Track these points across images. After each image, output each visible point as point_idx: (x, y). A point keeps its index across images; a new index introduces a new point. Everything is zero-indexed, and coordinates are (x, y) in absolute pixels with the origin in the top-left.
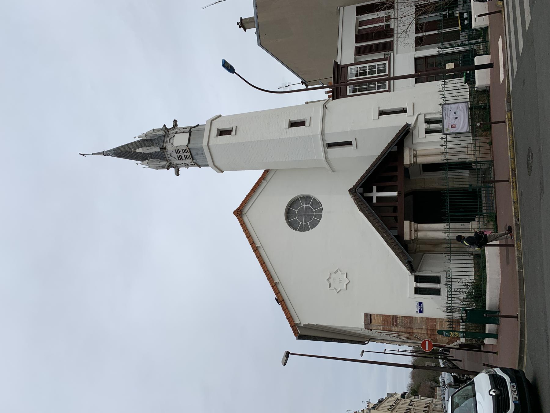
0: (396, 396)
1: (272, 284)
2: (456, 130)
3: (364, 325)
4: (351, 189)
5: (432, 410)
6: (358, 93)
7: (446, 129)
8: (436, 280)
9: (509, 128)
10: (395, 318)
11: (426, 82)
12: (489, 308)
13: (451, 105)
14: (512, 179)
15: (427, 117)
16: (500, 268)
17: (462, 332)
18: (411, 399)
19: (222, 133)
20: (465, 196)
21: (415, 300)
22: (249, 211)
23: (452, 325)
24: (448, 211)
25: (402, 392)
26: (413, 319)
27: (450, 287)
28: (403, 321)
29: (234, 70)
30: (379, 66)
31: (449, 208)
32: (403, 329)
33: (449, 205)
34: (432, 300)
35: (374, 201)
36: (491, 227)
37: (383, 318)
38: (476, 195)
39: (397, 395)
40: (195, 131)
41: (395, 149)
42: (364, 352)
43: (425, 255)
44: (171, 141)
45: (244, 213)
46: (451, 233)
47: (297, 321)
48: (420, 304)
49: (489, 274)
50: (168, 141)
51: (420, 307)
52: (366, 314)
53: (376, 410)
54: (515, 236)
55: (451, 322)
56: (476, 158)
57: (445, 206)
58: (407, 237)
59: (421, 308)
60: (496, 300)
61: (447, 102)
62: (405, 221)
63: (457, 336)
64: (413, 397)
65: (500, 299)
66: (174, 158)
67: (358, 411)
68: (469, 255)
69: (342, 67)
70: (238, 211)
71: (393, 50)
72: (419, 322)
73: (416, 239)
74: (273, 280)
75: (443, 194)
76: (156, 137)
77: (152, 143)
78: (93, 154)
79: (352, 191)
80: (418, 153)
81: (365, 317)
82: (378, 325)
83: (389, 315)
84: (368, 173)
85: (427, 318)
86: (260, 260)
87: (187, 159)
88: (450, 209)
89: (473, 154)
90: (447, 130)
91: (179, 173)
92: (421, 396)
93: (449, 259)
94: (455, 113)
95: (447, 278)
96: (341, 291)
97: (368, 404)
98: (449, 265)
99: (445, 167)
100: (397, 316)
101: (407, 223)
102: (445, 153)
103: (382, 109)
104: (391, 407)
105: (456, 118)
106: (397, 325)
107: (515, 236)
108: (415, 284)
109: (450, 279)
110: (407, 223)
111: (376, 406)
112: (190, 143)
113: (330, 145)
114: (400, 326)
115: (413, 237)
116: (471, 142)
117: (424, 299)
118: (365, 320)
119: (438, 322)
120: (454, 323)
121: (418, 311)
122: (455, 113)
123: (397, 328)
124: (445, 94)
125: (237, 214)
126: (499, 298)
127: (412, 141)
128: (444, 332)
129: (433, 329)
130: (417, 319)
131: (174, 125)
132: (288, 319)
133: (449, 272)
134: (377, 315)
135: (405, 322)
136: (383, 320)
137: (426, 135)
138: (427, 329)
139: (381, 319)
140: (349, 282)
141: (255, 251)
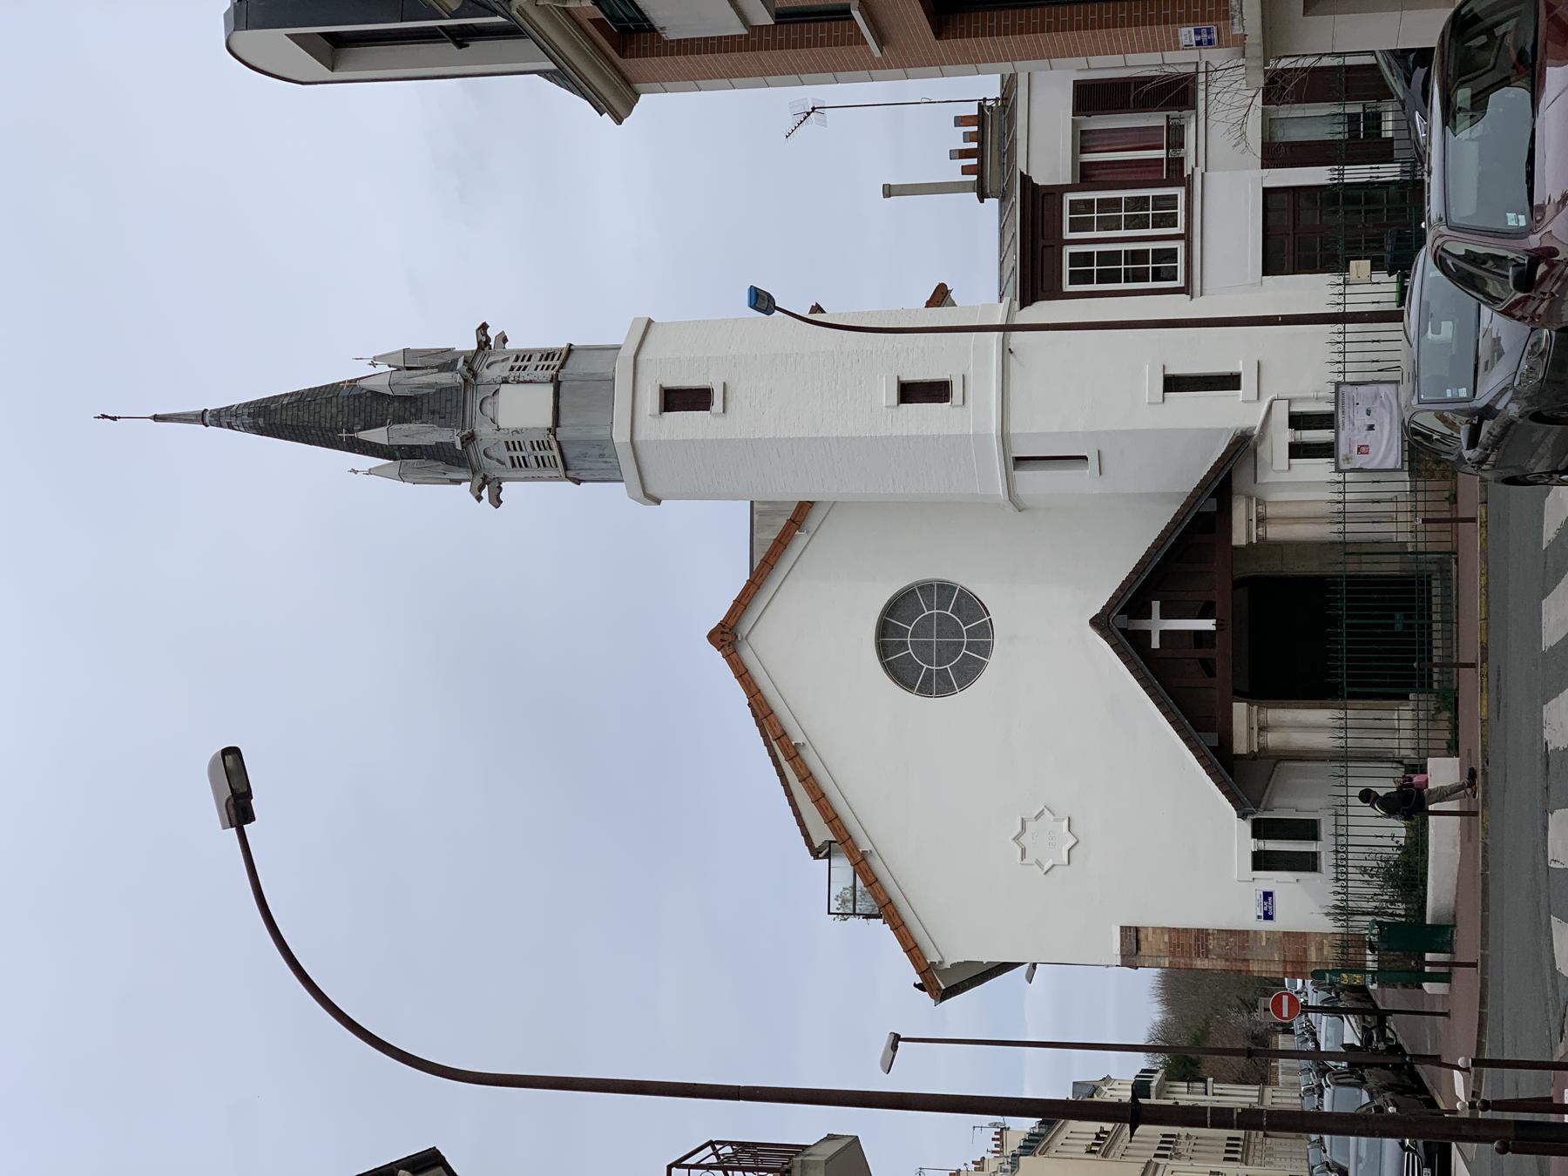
0: (1112, 1092)
1: (852, 857)
2: (1368, 463)
7: (1344, 455)
8: (1309, 830)
10: (1202, 935)
12: (1434, 916)
13: (1360, 388)
14: (1481, 667)
15: (1298, 408)
18: (1177, 1096)
19: (677, 399)
22: (756, 629)
24: (1342, 683)
25: (1138, 1073)
26: (1248, 935)
28: (1224, 943)
29: (770, 298)
32: (1223, 963)
33: (1347, 658)
34: (1297, 885)
35: (1155, 643)
36: (1445, 725)
37: (1170, 937)
39: (1115, 1086)
40: (575, 383)
41: (1212, 506)
43: (1281, 764)
44: (487, 407)
45: (742, 638)
47: (933, 957)
48: (1267, 895)
50: (484, 457)
51: (1266, 903)
52: (1124, 929)
53: (1039, 1158)
54: (1479, 795)
55: (1344, 947)
57: (1336, 669)
58: (1240, 747)
59: (1270, 907)
61: (1349, 378)
63: (1358, 981)
64: (1182, 1086)
65: (1457, 896)
66: (498, 461)
67: (964, 1168)
70: (722, 633)
71: (1194, 107)
72: (1264, 944)
73: (1263, 749)
74: (856, 847)
75: (1333, 636)
76: (426, 391)
77: (413, 410)
78: (156, 418)
80: (1271, 511)
81: (1121, 935)
82: (1157, 956)
84: (1142, 573)
85: (1284, 933)
90: (1347, 459)
93: (1340, 372)
94: (1368, 413)
97: (996, 1133)
100: (1207, 930)
101: (1240, 709)
103: (1175, 370)
104: (1098, 1138)
105: (1371, 428)
106: (1206, 955)
107: (1479, 795)
108: (1252, 845)
110: (1240, 709)
111: (1037, 1141)
113: (1020, 461)
114: (1215, 957)
115: (1256, 746)
116: (1406, 486)
118: (1122, 945)
119: (1313, 943)
120: (1351, 950)
121: (1262, 914)
123: (1206, 960)
125: (722, 640)
128: (1327, 975)
129: (1299, 960)
130: (1259, 936)
131: (479, 343)
133: (1343, 838)
135: (1227, 945)
136: (1170, 942)
138: (1285, 961)
139: (1166, 939)
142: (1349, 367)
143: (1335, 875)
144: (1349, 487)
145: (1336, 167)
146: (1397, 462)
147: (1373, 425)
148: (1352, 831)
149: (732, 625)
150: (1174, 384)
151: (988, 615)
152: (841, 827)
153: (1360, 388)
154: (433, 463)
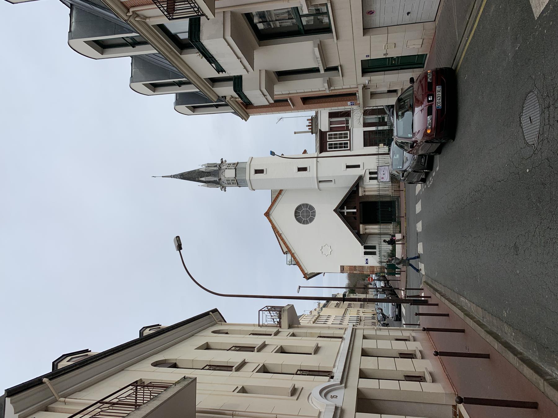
6: (333, 150)
8: (374, 247)
10: (355, 267)
15: (371, 171)
19: (257, 172)
21: (365, 258)
29: (274, 153)
30: (345, 134)
35: (345, 214)
38: (392, 204)
39: (340, 295)
41: (355, 189)
47: (306, 272)
48: (367, 259)
54: (405, 241)
58: (361, 233)
62: (360, 225)
71: (351, 116)
78: (163, 177)
80: (366, 190)
88: (381, 219)
91: (226, 190)
94: (383, 171)
95: (379, 251)
101: (361, 226)
102: (379, 190)
104: (337, 304)
105: (384, 174)
107: (405, 241)
108: (364, 250)
110: (361, 226)
113: (320, 181)
122: (383, 171)
131: (221, 162)
134: (346, 266)
142: (380, 187)
144: (380, 185)
148: (382, 247)
150: (348, 167)
154: (213, 184)
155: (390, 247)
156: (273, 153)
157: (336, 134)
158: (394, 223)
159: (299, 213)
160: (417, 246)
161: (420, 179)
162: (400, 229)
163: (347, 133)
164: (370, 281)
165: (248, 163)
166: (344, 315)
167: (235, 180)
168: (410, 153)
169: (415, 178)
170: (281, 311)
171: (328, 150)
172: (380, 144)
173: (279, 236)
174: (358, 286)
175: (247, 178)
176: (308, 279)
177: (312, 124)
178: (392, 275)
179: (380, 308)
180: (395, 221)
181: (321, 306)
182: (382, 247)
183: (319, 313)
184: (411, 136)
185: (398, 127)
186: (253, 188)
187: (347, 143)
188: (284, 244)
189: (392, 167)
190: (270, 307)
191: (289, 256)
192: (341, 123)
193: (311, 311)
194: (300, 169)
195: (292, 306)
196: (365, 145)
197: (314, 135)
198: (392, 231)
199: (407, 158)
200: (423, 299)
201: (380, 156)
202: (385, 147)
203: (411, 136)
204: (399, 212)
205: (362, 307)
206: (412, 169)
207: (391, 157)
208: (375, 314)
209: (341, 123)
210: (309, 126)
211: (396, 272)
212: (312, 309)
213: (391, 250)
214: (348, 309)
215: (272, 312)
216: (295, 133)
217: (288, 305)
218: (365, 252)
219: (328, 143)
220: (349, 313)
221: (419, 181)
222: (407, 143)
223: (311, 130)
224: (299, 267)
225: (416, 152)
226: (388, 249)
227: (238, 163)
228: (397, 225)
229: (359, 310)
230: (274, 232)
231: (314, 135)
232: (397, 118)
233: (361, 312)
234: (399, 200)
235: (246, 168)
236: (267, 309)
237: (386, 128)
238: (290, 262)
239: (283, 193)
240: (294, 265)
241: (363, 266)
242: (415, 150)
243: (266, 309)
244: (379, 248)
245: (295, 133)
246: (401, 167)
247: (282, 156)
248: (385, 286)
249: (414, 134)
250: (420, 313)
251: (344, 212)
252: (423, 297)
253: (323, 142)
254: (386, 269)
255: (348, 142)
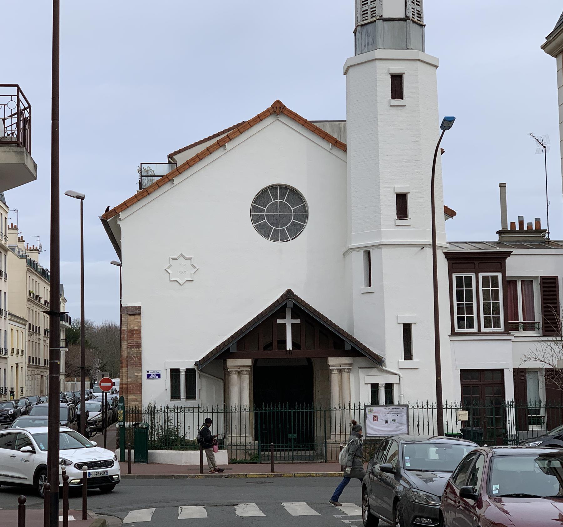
3: (126, 306)
4: (292, 293)
5: (42, 374)
6: (455, 289)
8: (191, 395)
9: (331, 474)
11: (461, 384)
12: (152, 453)
13: (406, 416)
14: (272, 474)
15: (395, 387)
16: (194, 464)
17: (124, 423)
20: (282, 430)
23: (132, 413)
24: (262, 410)
26: (139, 367)
27: (179, 412)
28: (135, 355)
29: (449, 128)
31: (282, 411)
32: (125, 355)
33: (267, 412)
34: (164, 389)
35: (279, 321)
36: (243, 457)
41: (347, 347)
42: (120, 267)
43: (222, 382)
46: (207, 413)
47: (123, 215)
49: (187, 453)
51: (155, 375)
52: (139, 308)
53: (26, 268)
54: (210, 474)
55: (135, 412)
56: (331, 444)
58: (230, 363)
60: (160, 460)
61: (410, 412)
63: (119, 418)
67: (19, 232)
68: (223, 435)
69: (501, 263)
70: (280, 108)
71: (544, 335)
72: (136, 374)
74: (176, 176)
75: (302, 405)
79: (289, 294)
80: (345, 375)
83: (141, 338)
86: (204, 153)
87: (363, 14)
89: (337, 440)
90: (371, 411)
92: (66, 351)
95: (181, 408)
96: (167, 273)
97: (36, 247)
98: (210, 410)
99: (264, 409)
100: (141, 347)
101: (248, 362)
102: (343, 409)
103: (414, 329)
104: (37, 296)
105: (386, 422)
107: (210, 474)
108: (183, 369)
109: (180, 411)
110: (248, 362)
112: (385, 23)
113: (368, 254)
114: (128, 351)
115: (231, 370)
117: (165, 380)
118: (132, 307)
121: (149, 373)
123: (126, 347)
124: (423, 409)
125: (276, 108)
126: (162, 464)
127: (369, 366)
128: (122, 404)
129: (129, 391)
132: (124, 203)
134: (140, 322)
135: (134, 357)
137: (370, 385)
138: (127, 384)
140: (182, 285)
141: (218, 143)
142: (352, 412)
143: (170, 407)
145: (514, 404)
146: (370, 434)
147: (387, 423)
149: (284, 112)
150: (407, 328)
151: (292, 239)
152: (185, 169)
153: (405, 417)
155: (193, 435)
156: (447, 123)
157: (496, 297)
158: (257, 447)
159: (282, 197)
160: (197, 505)
161: (376, 514)
162: (241, 462)
163: (499, 327)
164: (102, 384)
165: (421, 56)
166: (8, 317)
167: (374, 19)
168: (446, 488)
169: (379, 501)
170: (18, 145)
171: (454, 276)
172: (467, 412)
173: (218, 142)
174: (87, 352)
175: (378, 53)
176: (104, 221)
177: (526, 232)
178: (118, 440)
179: (31, 409)
180: (262, 449)
181: (33, 256)
182: (191, 415)
183: (13, 249)
184: (494, 492)
185: (523, 458)
186: (351, 70)
187: (471, 326)
188: (197, 156)
189: (408, 442)
190: (27, 115)
191: (164, 170)
192: (529, 310)
193: (16, 228)
194: (402, 199)
195: (32, 175)
196: (465, 373)
197: (496, 238)
198: (234, 441)
199: (432, 480)
200: (61, 518)
201: (435, 411)
202: (460, 426)
203: (494, 492)
204: (285, 460)
205: (31, 363)
206: (403, 493)
207: (434, 440)
208: (13, 395)
209: (529, 310)
210: (521, 223)
211: (127, 451)
212: (23, 231)
213: (184, 437)
214: (25, 325)
215: (15, 120)
216: (502, 186)
217: (35, 166)
218: (180, 372)
219: (473, 275)
220: (15, 329)
221: (371, 511)
222: (474, 480)
223: (509, 229)
224: (136, 196)
225: (450, 504)
226: (187, 431)
227: (422, 26)
228: (250, 455)
229: (22, 354)
230: (229, 130)
231: (496, 238)
232: (541, 455)
233: (19, 359)
234: (317, 459)
235: (408, 49)
236: (22, 108)
237: (511, 429)
238: (147, 171)
239: (338, 152)
240: (140, 183)
241: (140, 366)
242: (455, 501)
243: (25, 104)
244: (189, 408)
245: (502, 186)
246: (408, 465)
247: (438, 151)
248: (90, 423)
249: (498, 499)
250: (26, 510)
251: (284, 318)
252: (65, 518)
253: (477, 262)
254: (135, 425)
255: (475, 329)
